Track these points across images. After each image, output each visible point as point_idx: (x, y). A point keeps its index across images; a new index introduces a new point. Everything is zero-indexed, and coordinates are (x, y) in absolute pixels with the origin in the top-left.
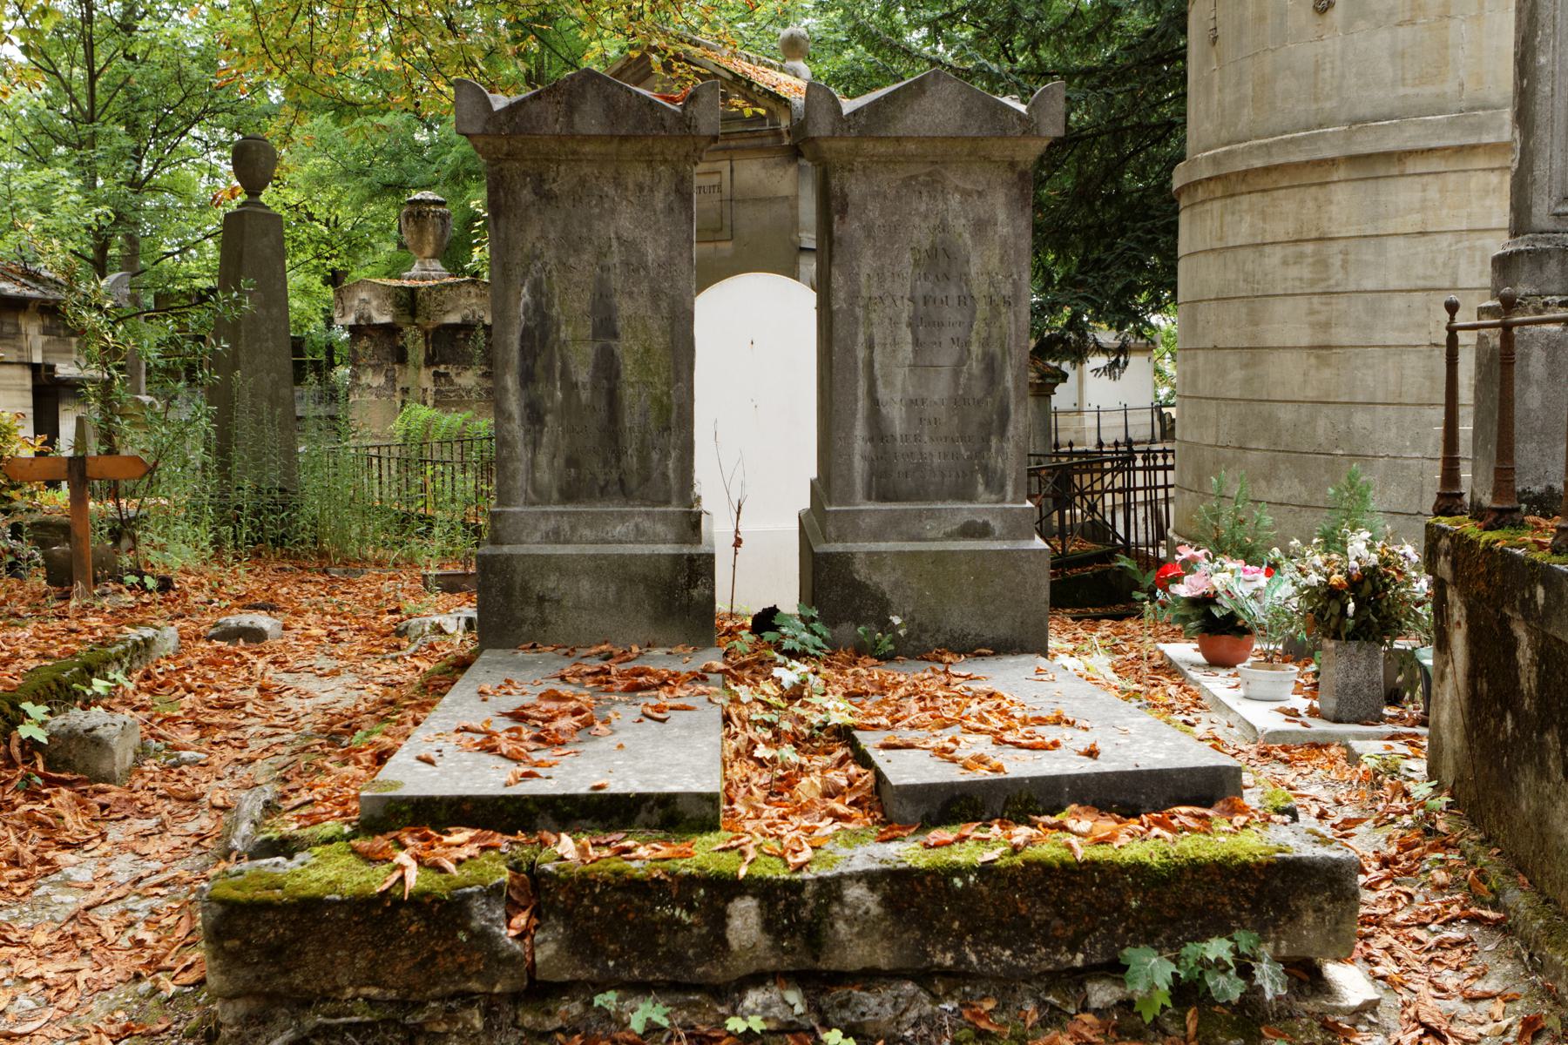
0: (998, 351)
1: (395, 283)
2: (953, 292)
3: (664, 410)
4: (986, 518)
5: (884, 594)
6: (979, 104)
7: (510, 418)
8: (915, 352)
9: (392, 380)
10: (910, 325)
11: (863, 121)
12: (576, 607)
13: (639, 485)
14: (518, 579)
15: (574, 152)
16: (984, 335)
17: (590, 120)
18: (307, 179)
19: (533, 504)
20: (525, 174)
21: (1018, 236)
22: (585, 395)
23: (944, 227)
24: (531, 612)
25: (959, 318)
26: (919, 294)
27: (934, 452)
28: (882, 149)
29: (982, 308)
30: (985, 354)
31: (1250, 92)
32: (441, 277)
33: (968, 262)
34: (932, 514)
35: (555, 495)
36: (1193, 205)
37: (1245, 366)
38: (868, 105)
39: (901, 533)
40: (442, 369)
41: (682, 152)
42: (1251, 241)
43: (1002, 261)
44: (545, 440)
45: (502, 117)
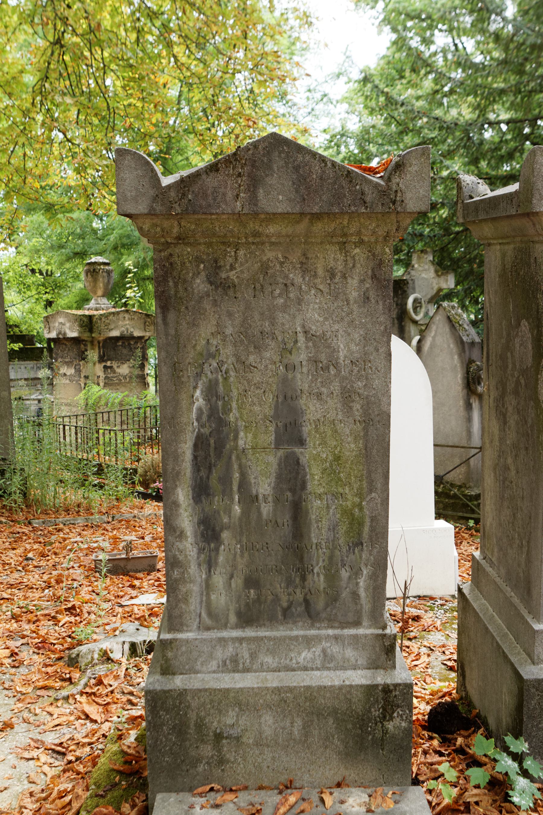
1: (80, 312)
3: (355, 523)
7: (181, 535)
9: (78, 371)
12: (257, 744)
13: (327, 605)
14: (192, 716)
15: (256, 234)
17: (277, 196)
18: (30, 251)
19: (208, 629)
20: (198, 260)
22: (266, 509)
24: (207, 750)
32: (108, 308)
35: (233, 619)
40: (109, 364)
41: (381, 232)
44: (221, 559)
45: (173, 194)
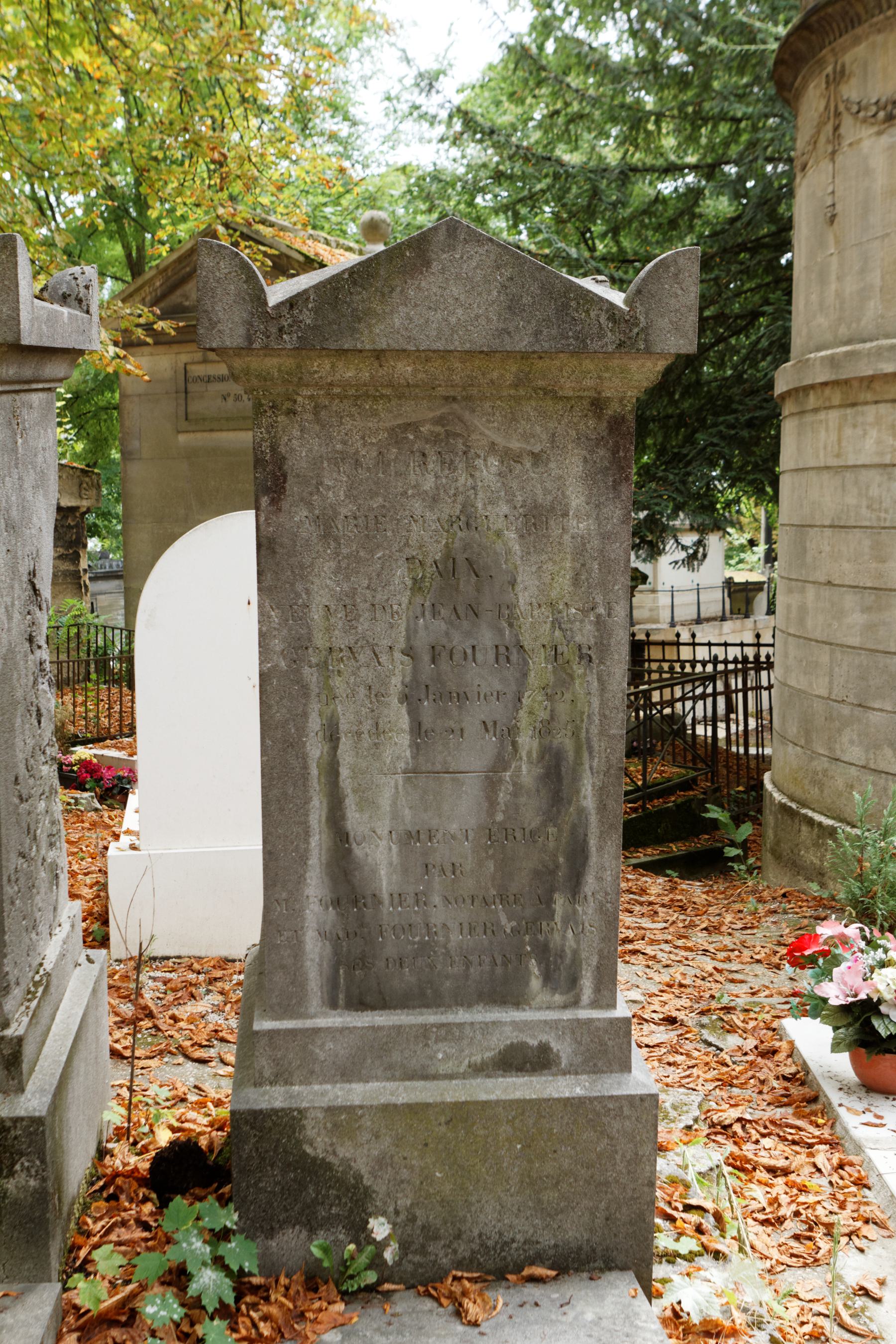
0: (569, 745)
2: (487, 638)
4: (544, 1038)
5: (359, 1177)
6: (535, 288)
8: (416, 747)
10: (405, 698)
11: (307, 318)
16: (544, 715)
21: (606, 537)
23: (467, 519)
25: (497, 686)
26: (422, 642)
27: (450, 924)
28: (348, 372)
29: (540, 667)
30: (545, 750)
31: (878, 282)
33: (513, 583)
34: (448, 1032)
36: (802, 413)
37: (866, 610)
38: (317, 287)
39: (390, 1067)
42: (876, 460)
43: (576, 581)
